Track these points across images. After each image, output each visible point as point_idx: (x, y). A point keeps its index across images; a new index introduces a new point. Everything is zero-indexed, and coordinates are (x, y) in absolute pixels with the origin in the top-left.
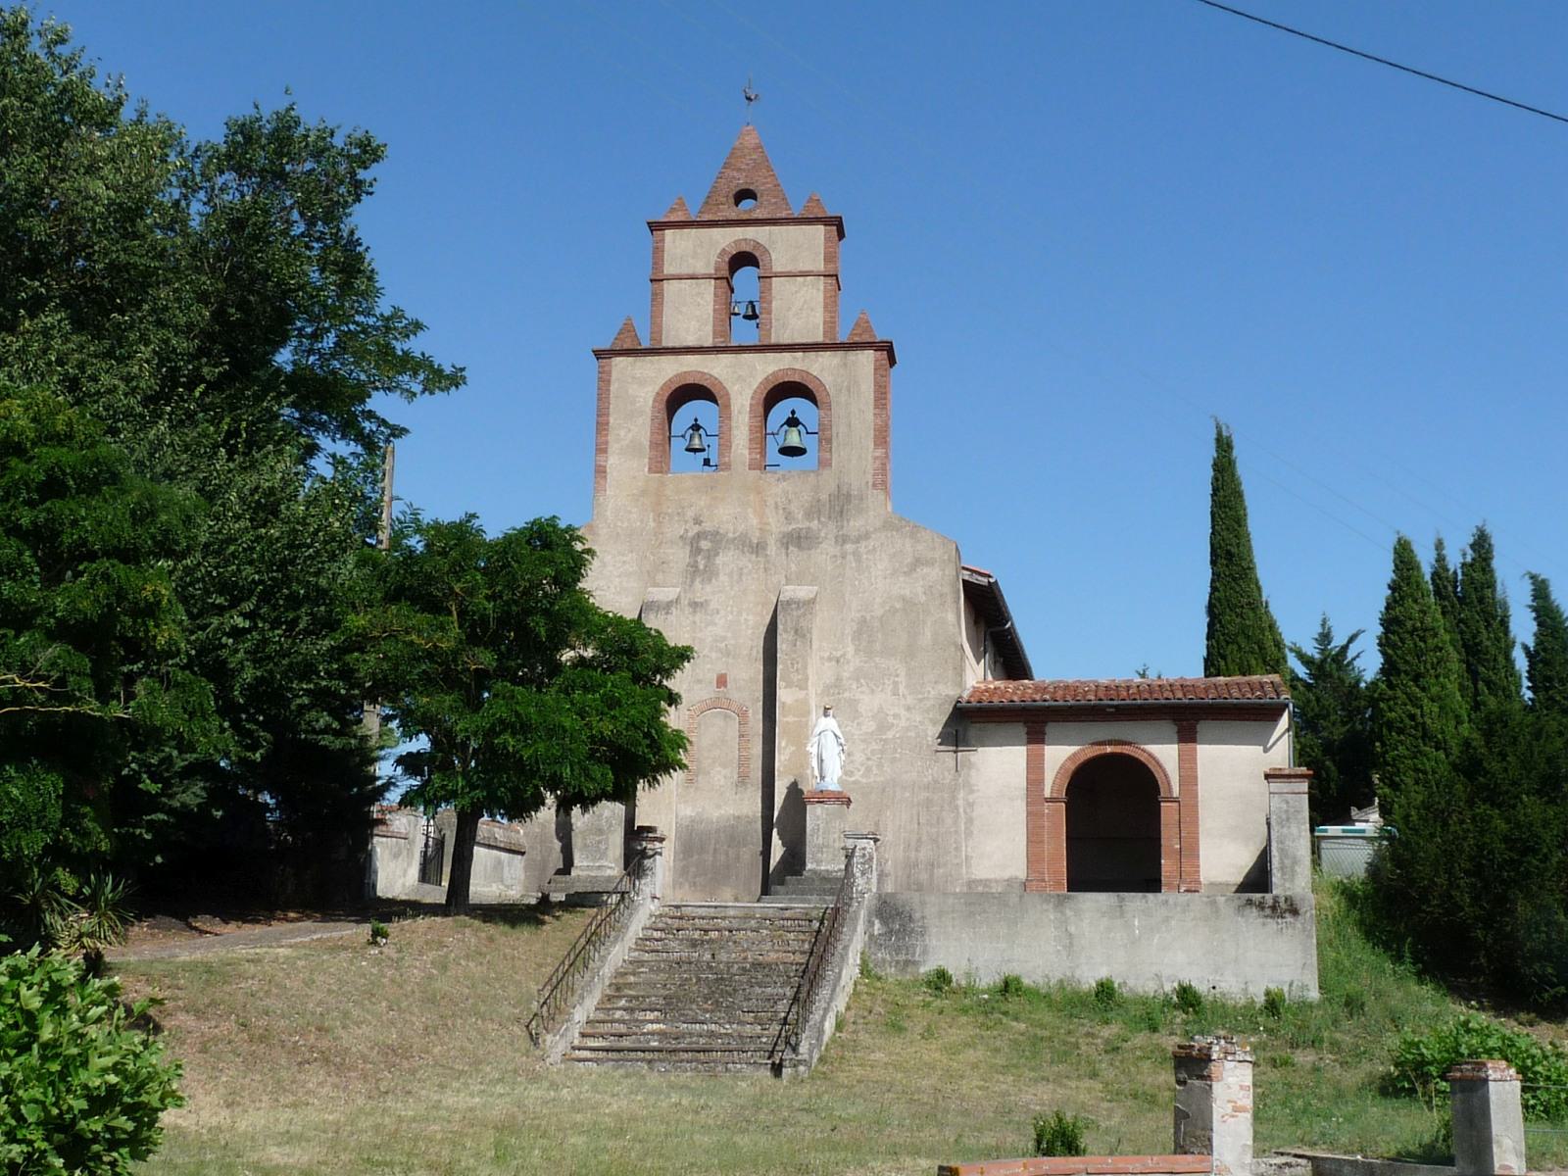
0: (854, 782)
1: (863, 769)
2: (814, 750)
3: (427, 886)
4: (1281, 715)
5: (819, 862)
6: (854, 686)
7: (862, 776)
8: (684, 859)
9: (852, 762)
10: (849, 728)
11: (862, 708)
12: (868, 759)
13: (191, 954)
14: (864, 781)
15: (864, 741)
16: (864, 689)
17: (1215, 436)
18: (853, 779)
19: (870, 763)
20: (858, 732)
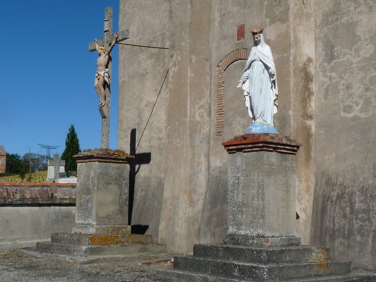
0: (354, 119)
1: (361, 102)
2: (248, 104)
3: (77, 205)
4: (275, 62)
5: (239, 225)
6: (352, 8)
7: (361, 111)
8: (211, 208)
9: (350, 95)
10: (348, 56)
11: (360, 31)
12: (367, 90)
13: (179, 273)
14: (363, 116)
15: (362, 69)
16: (363, 8)
17: (91, 52)
18: (351, 115)
19: (369, 94)
20: (355, 60)
